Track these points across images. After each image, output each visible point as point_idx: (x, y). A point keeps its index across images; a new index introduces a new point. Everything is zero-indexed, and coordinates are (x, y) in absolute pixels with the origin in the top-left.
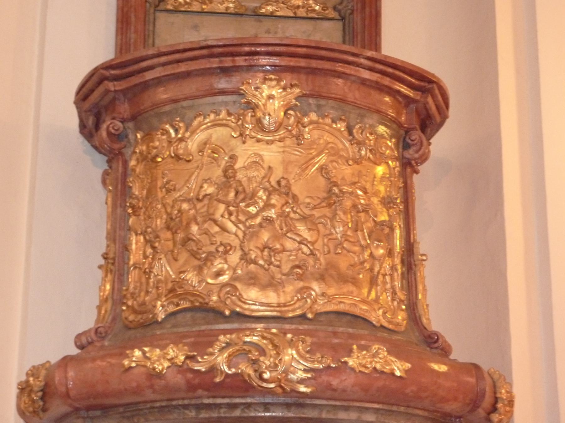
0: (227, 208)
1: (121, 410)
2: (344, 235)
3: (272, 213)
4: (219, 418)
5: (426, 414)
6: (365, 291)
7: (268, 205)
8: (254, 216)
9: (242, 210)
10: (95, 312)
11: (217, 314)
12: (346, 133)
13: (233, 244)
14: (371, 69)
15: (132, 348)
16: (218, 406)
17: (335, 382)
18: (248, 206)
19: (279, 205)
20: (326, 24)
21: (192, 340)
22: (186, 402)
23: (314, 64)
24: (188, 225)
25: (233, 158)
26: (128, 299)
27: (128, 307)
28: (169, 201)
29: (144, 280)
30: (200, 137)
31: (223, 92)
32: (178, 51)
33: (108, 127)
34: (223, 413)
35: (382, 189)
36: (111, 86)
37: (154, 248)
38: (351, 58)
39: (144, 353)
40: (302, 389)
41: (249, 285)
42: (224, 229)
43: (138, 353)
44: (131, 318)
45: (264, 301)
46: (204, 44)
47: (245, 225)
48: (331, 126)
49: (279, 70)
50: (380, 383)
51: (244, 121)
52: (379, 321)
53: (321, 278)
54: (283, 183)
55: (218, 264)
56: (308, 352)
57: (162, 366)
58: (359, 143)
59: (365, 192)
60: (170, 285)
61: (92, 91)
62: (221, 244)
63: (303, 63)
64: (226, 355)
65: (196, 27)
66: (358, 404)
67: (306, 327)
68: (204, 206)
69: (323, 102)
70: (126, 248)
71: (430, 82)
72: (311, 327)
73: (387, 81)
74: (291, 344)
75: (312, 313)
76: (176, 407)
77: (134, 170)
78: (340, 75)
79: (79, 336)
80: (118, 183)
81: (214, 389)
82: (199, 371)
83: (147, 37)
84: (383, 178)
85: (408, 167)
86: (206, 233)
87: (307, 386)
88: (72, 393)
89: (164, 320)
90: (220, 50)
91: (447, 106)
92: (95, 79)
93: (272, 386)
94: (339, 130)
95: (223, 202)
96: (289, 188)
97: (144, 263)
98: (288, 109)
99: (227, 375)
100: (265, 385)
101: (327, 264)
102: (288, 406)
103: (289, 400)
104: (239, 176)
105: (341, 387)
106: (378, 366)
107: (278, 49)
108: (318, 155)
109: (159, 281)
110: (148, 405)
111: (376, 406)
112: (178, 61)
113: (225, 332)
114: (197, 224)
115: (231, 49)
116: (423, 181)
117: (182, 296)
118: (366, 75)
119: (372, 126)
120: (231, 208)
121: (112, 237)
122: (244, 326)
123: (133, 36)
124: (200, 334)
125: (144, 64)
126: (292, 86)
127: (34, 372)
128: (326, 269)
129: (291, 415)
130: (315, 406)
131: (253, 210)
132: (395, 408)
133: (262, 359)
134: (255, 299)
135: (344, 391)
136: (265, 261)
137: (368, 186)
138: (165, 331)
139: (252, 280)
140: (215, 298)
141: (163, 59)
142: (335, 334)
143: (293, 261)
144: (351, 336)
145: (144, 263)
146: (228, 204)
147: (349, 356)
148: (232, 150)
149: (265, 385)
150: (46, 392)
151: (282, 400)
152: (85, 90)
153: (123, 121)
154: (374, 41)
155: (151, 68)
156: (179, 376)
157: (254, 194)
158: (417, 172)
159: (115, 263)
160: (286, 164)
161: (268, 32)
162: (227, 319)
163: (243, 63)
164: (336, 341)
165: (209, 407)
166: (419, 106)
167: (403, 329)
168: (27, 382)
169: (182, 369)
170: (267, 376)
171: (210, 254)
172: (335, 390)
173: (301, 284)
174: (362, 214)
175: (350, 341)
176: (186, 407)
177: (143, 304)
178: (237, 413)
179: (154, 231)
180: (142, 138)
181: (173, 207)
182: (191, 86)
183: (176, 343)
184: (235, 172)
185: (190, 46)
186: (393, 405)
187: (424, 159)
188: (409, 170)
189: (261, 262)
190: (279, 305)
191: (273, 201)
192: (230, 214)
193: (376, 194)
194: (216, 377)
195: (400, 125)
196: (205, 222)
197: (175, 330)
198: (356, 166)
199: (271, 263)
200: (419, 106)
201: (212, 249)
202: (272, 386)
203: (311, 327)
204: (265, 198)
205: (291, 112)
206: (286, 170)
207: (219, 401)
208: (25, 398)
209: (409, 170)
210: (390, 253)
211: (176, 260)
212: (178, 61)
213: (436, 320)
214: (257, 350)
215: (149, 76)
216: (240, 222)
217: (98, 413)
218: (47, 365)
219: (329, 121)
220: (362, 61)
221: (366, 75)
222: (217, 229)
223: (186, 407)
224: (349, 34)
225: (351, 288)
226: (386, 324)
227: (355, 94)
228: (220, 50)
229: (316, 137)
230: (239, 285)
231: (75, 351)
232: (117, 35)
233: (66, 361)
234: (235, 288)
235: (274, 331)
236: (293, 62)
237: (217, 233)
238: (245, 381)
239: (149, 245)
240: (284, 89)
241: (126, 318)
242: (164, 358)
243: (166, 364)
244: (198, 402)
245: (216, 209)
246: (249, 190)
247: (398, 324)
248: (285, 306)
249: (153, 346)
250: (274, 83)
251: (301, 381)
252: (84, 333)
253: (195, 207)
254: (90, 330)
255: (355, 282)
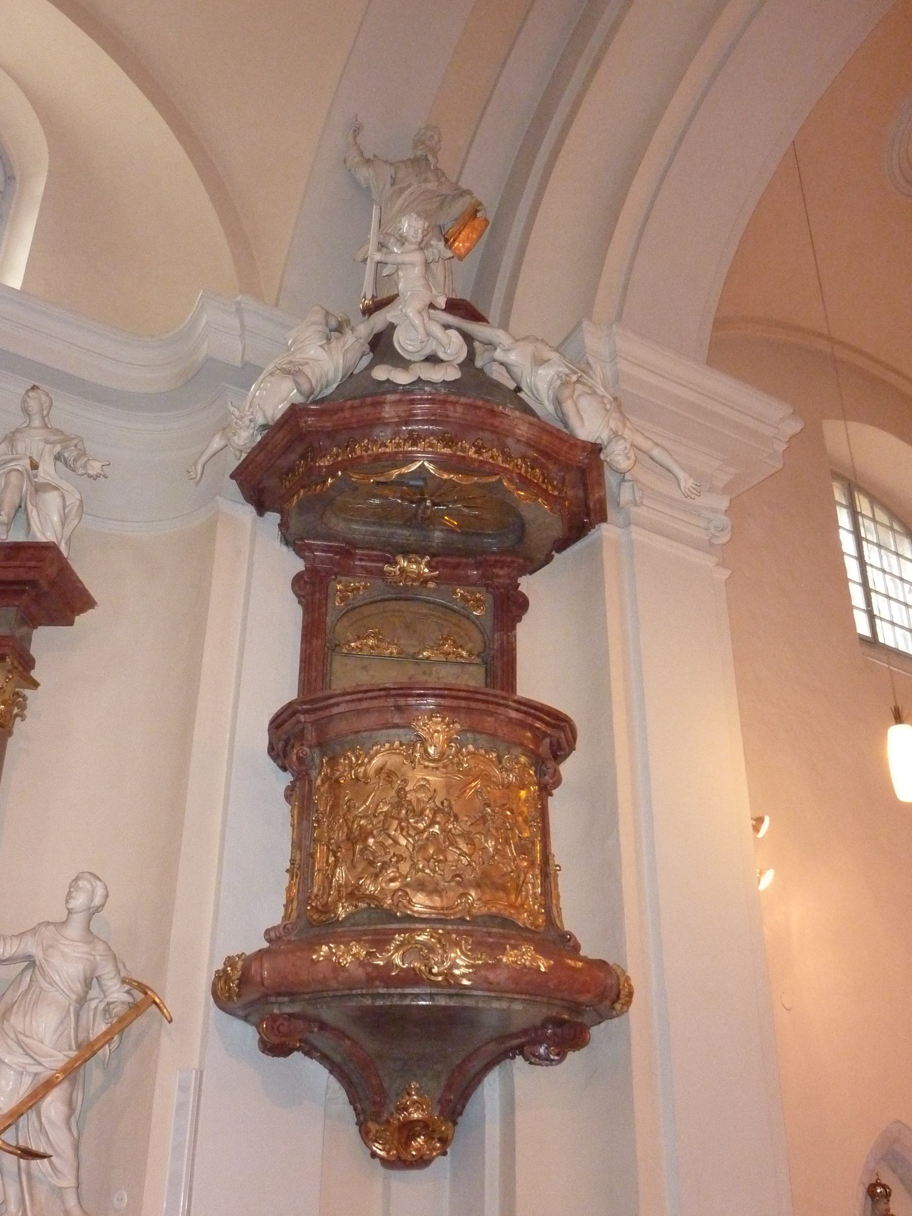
0: (399, 824)
1: (307, 997)
2: (496, 850)
3: (436, 829)
4: (391, 1006)
5: (565, 1004)
6: (513, 897)
7: (432, 823)
8: (423, 831)
9: (412, 827)
10: (283, 909)
11: (390, 916)
12: (496, 762)
13: (404, 855)
14: (517, 710)
15: (321, 945)
16: (391, 995)
17: (491, 976)
18: (416, 822)
19: (443, 823)
20: (472, 668)
21: (370, 937)
22: (364, 991)
23: (473, 705)
24: (366, 839)
25: (405, 781)
26: (313, 901)
27: (312, 907)
28: (350, 817)
29: (326, 885)
30: (376, 762)
31: (397, 726)
32: (361, 692)
33: (297, 753)
34: (396, 1001)
35: (525, 809)
36: (302, 718)
37: (335, 855)
38: (502, 701)
39: (330, 948)
40: (465, 982)
41: (418, 891)
42: (396, 842)
43: (325, 948)
44: (315, 917)
45: (431, 904)
46: (382, 686)
47: (414, 840)
48: (484, 756)
49: (440, 709)
50: (527, 978)
51: (414, 751)
52: (524, 924)
53: (478, 886)
54: (446, 804)
55: (391, 873)
56: (469, 951)
57: (347, 961)
58: (507, 770)
59: (512, 812)
60: (350, 889)
61: (285, 721)
62: (394, 855)
63: (463, 704)
64: (401, 952)
65: (365, 668)
66: (509, 995)
67: (465, 927)
68: (379, 823)
69: (478, 736)
70: (312, 856)
71: (566, 721)
72: (469, 928)
73: (529, 720)
74: (457, 944)
75: (470, 915)
76: (354, 995)
77: (318, 789)
78: (491, 714)
79: (267, 932)
80: (300, 796)
81: (389, 982)
82: (378, 965)
83: (325, 675)
84: (526, 800)
85: (545, 790)
86: (382, 844)
87: (469, 980)
88: (266, 983)
89: (345, 919)
90: (394, 692)
91: (575, 739)
92: (289, 711)
93: (440, 978)
94: (491, 760)
95: (397, 819)
96: (451, 808)
97: (327, 870)
98: (449, 740)
99: (402, 970)
100: (432, 978)
101: (483, 873)
102: (451, 996)
103: (451, 991)
104: (409, 797)
105: (496, 980)
106: (527, 963)
107: (441, 692)
108: (474, 781)
109: (340, 886)
110: (331, 994)
111: (524, 997)
112: (360, 700)
113: (400, 931)
114: (374, 837)
115: (404, 691)
116: (557, 804)
117: (360, 899)
118: (513, 714)
119: (517, 757)
120: (403, 824)
121: (297, 845)
122: (412, 926)
123: (314, 674)
124: (376, 932)
125: (332, 701)
126: (453, 723)
127: (230, 961)
128: (481, 878)
129: (452, 1004)
130: (472, 996)
131: (421, 826)
132: (539, 999)
133: (431, 956)
134: (420, 903)
135: (498, 984)
136: (431, 871)
137: (514, 807)
138: (346, 929)
139: (421, 886)
140: (389, 902)
141: (348, 698)
142: (489, 934)
143: (454, 870)
144: (503, 936)
145: (327, 870)
146: (400, 821)
147: (503, 954)
148: (404, 775)
149: (432, 978)
150: (244, 980)
151: (445, 991)
152: (279, 720)
153: (310, 747)
154: (510, 684)
155: (337, 704)
156: (360, 969)
157: (422, 813)
158: (551, 795)
159: (301, 869)
160: (448, 787)
161: (424, 673)
162: (399, 920)
163: (414, 702)
164: (491, 940)
165: (382, 996)
166: (549, 737)
167: (542, 929)
168: (225, 971)
169: (362, 964)
170: (435, 970)
171: (384, 863)
172: (491, 983)
173: (461, 890)
174: (509, 832)
175: (502, 941)
176: (363, 995)
177: (326, 905)
178: (407, 1002)
179: (336, 843)
180: (327, 762)
181: (353, 822)
182: (371, 720)
183: (358, 942)
184: (406, 793)
185: (370, 688)
186: (537, 995)
187: (557, 782)
188: (544, 793)
189: (427, 871)
190: (442, 908)
191: (438, 819)
192: (402, 829)
193: (521, 814)
194: (392, 971)
195: (538, 756)
196: (379, 835)
197: (354, 928)
198: (505, 791)
199: (435, 872)
200: (549, 737)
201: (387, 858)
202: (440, 978)
203: (469, 928)
204: (431, 816)
205: (453, 744)
206: (448, 793)
207: (392, 991)
208: (221, 984)
209: (544, 793)
210: (532, 864)
211: (355, 867)
212: (360, 700)
213: (570, 922)
214: (427, 949)
215: (335, 710)
216: (410, 836)
217: (286, 999)
218: (243, 957)
219: (482, 752)
220: (511, 703)
221: (513, 714)
222: (390, 842)
223: (363, 995)
224: (491, 677)
225: (501, 894)
226: (528, 926)
227: (503, 731)
228: (394, 692)
229: (473, 765)
230: (409, 891)
231: (266, 945)
232: (300, 673)
233: (261, 954)
234: (407, 894)
235: (440, 931)
236: (455, 703)
237: (390, 845)
238: (416, 974)
239: (331, 853)
240: (448, 725)
241: (311, 917)
242: (349, 955)
243: (349, 959)
244: (375, 991)
245: (391, 823)
246: (418, 809)
247: (537, 927)
248: (447, 909)
249: (338, 944)
250: (439, 719)
251: (464, 975)
252: (274, 928)
253: (372, 823)
254: (279, 926)
255: (504, 889)
